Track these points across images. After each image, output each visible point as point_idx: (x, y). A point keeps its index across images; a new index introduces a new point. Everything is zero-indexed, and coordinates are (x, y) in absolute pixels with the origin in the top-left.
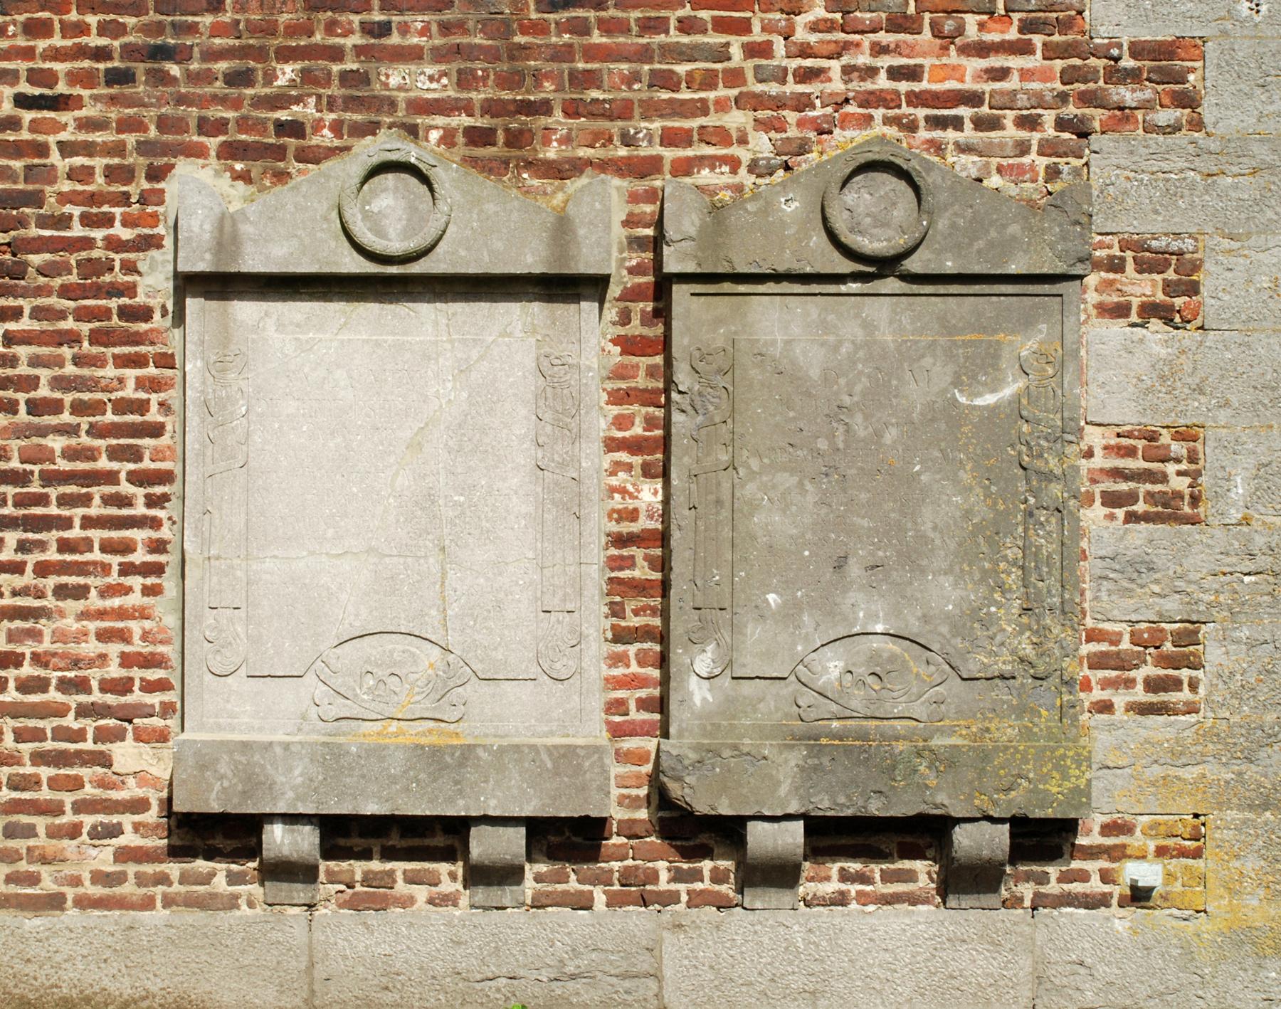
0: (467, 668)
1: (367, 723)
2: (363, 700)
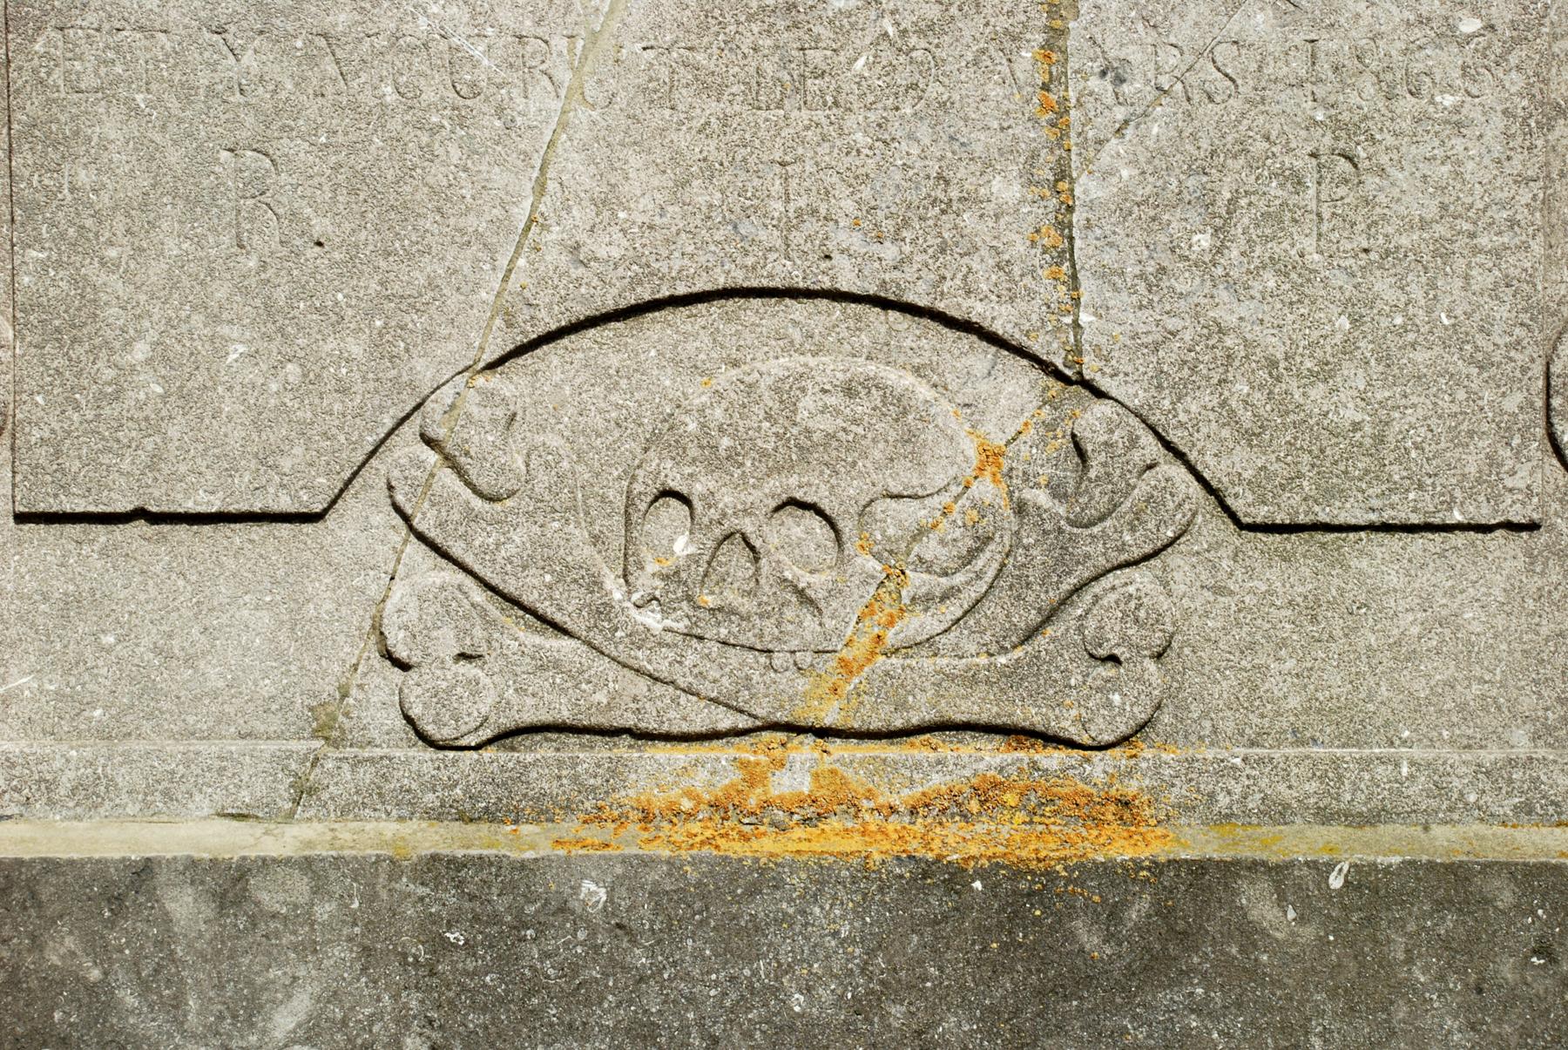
0: (1179, 472)
1: (661, 753)
2: (640, 638)
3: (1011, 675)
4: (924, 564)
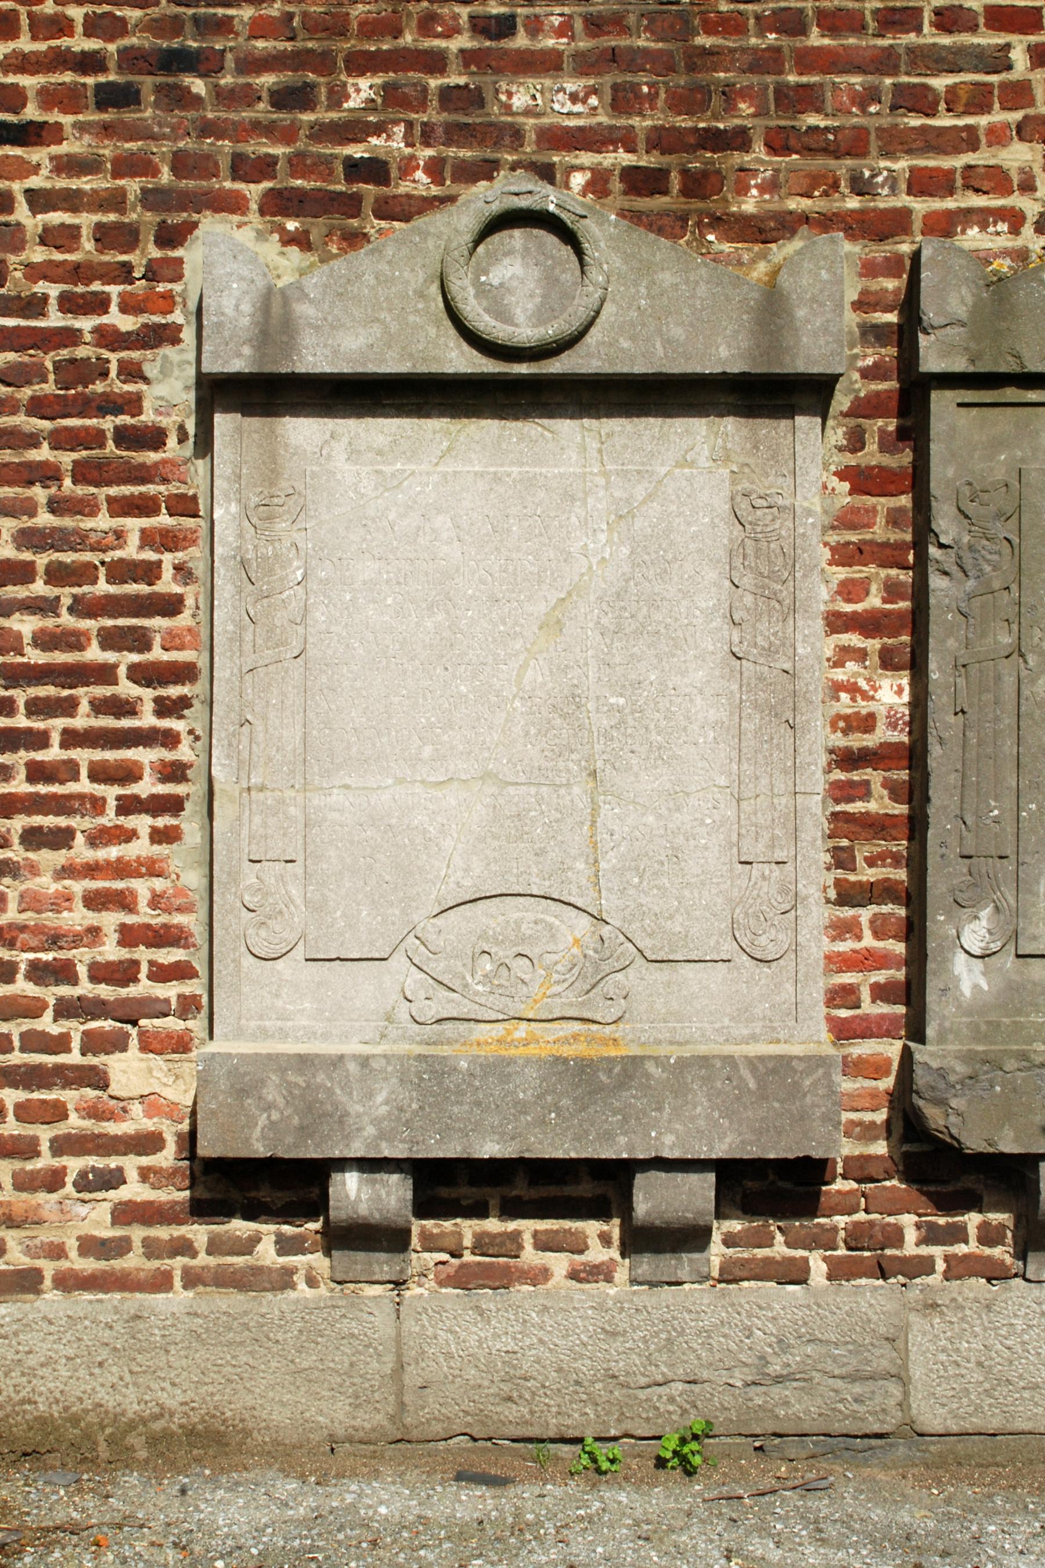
0: (630, 945)
1: (483, 1026)
2: (477, 993)
3: (583, 1003)
4: (557, 972)
